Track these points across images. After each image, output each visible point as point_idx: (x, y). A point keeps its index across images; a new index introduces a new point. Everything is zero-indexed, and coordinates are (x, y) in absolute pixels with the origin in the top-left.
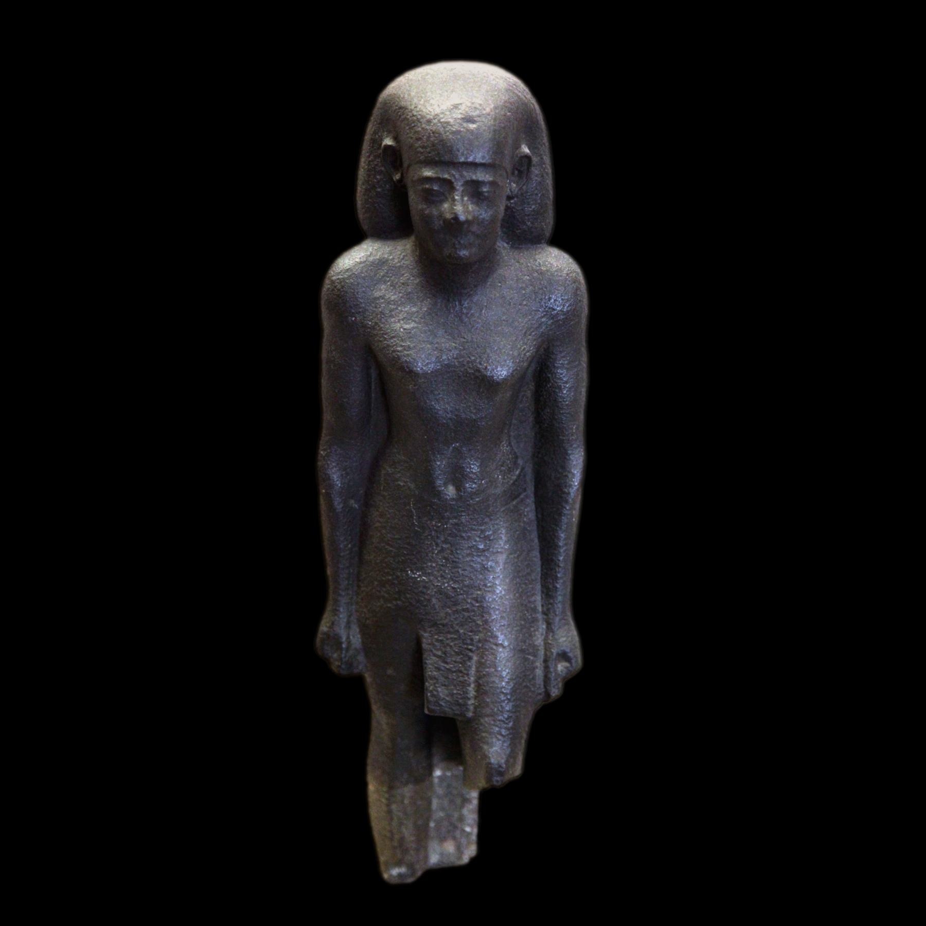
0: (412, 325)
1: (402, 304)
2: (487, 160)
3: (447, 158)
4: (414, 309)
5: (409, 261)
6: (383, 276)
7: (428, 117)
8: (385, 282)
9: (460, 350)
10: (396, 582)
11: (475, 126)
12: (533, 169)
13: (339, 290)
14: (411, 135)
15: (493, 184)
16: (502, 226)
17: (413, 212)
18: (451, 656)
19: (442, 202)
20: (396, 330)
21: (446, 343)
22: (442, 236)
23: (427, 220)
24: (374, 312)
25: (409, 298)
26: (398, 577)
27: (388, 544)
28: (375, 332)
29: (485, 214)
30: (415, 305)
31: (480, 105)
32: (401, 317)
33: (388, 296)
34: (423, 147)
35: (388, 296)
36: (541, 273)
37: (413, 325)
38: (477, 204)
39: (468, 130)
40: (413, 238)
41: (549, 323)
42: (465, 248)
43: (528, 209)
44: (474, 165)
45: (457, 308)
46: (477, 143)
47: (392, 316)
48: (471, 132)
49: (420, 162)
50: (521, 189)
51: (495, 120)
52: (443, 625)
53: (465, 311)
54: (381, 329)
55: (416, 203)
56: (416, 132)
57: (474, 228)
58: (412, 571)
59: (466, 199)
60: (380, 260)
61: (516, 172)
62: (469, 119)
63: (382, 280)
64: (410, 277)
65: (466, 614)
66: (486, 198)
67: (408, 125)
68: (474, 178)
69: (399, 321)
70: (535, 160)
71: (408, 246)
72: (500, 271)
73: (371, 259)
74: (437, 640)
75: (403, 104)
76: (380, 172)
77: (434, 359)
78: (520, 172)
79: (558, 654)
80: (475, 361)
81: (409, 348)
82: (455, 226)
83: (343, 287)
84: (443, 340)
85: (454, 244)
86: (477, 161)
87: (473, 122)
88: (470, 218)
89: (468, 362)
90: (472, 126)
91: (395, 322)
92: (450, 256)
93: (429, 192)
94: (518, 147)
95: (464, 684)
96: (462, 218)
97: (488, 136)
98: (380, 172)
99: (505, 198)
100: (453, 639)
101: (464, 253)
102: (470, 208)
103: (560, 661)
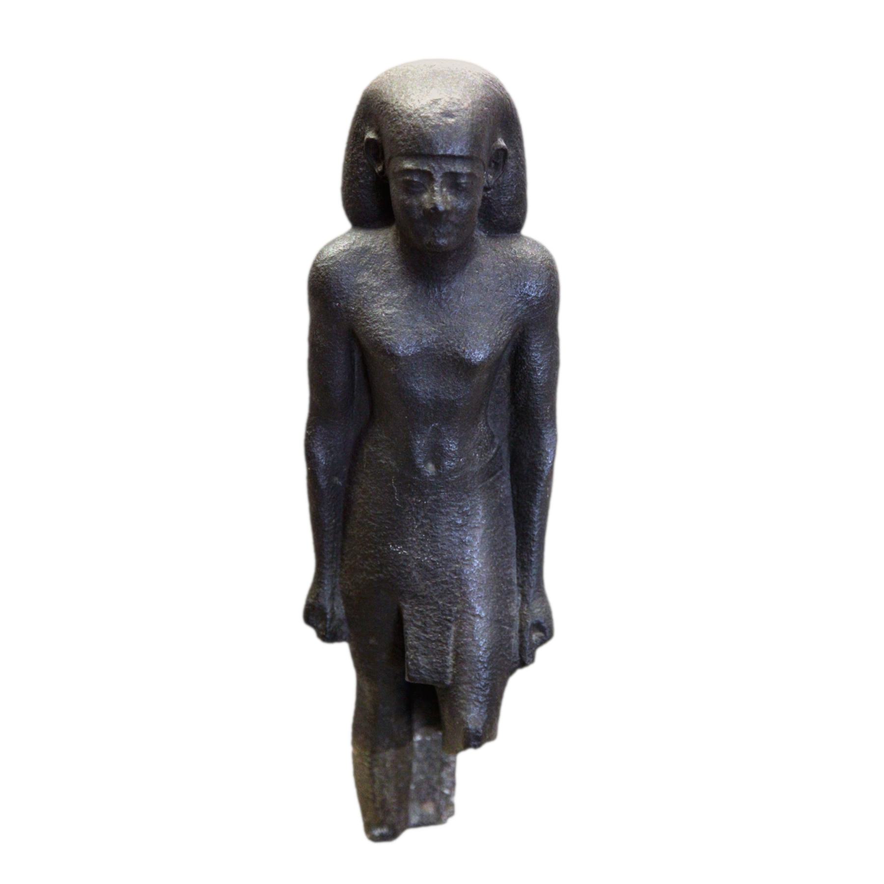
0: (393, 311)
1: (384, 290)
2: (465, 153)
3: (426, 151)
4: (395, 295)
5: (391, 249)
6: (366, 264)
7: (409, 111)
8: (368, 269)
9: (439, 334)
10: (378, 555)
11: (453, 120)
12: (509, 161)
13: (323, 277)
14: (392, 129)
15: (470, 175)
16: (480, 216)
17: (394, 203)
18: (431, 626)
19: (422, 192)
20: (378, 315)
21: (425, 327)
22: (422, 225)
23: (407, 210)
24: (357, 297)
25: (390, 284)
26: (380, 551)
27: (371, 520)
28: (358, 317)
29: (463, 204)
30: (396, 291)
31: (459, 100)
32: (383, 302)
33: (370, 283)
34: (404, 140)
35: (370, 283)
36: (517, 261)
37: (394, 310)
38: (456, 195)
39: (446, 124)
40: (394, 227)
41: (524, 308)
42: (444, 236)
43: (504, 200)
44: (453, 158)
45: (437, 294)
46: (455, 137)
47: (374, 302)
48: (450, 126)
49: (401, 155)
50: (497, 180)
51: (473, 114)
52: (423, 597)
53: (444, 297)
54: (363, 314)
55: (397, 193)
56: (397, 126)
57: (453, 218)
58: (393, 545)
59: (444, 190)
60: (363, 248)
61: (493, 164)
62: (448, 114)
63: (365, 268)
64: (391, 265)
65: (445, 586)
66: (464, 189)
67: (389, 119)
68: (453, 170)
69: (381, 307)
70: (511, 152)
71: (390, 235)
72: (478, 259)
73: (354, 247)
74: (417, 611)
75: (385, 99)
76: (363, 165)
77: (414, 343)
78: (497, 164)
79: (533, 625)
80: (453, 344)
81: (391, 332)
82: (434, 216)
83: (327, 274)
84: (423, 325)
85: (434, 233)
86: (455, 153)
87: (452, 116)
88: (449, 208)
89: (447, 346)
90: (451, 121)
91: (377, 308)
92: (429, 245)
93: (410, 183)
94: (494, 140)
95: (443, 653)
96: (441, 208)
97: (465, 129)
98: (363, 165)
99: (482, 189)
100: (432, 610)
101: (443, 241)
102: (449, 199)
103: (534, 631)
